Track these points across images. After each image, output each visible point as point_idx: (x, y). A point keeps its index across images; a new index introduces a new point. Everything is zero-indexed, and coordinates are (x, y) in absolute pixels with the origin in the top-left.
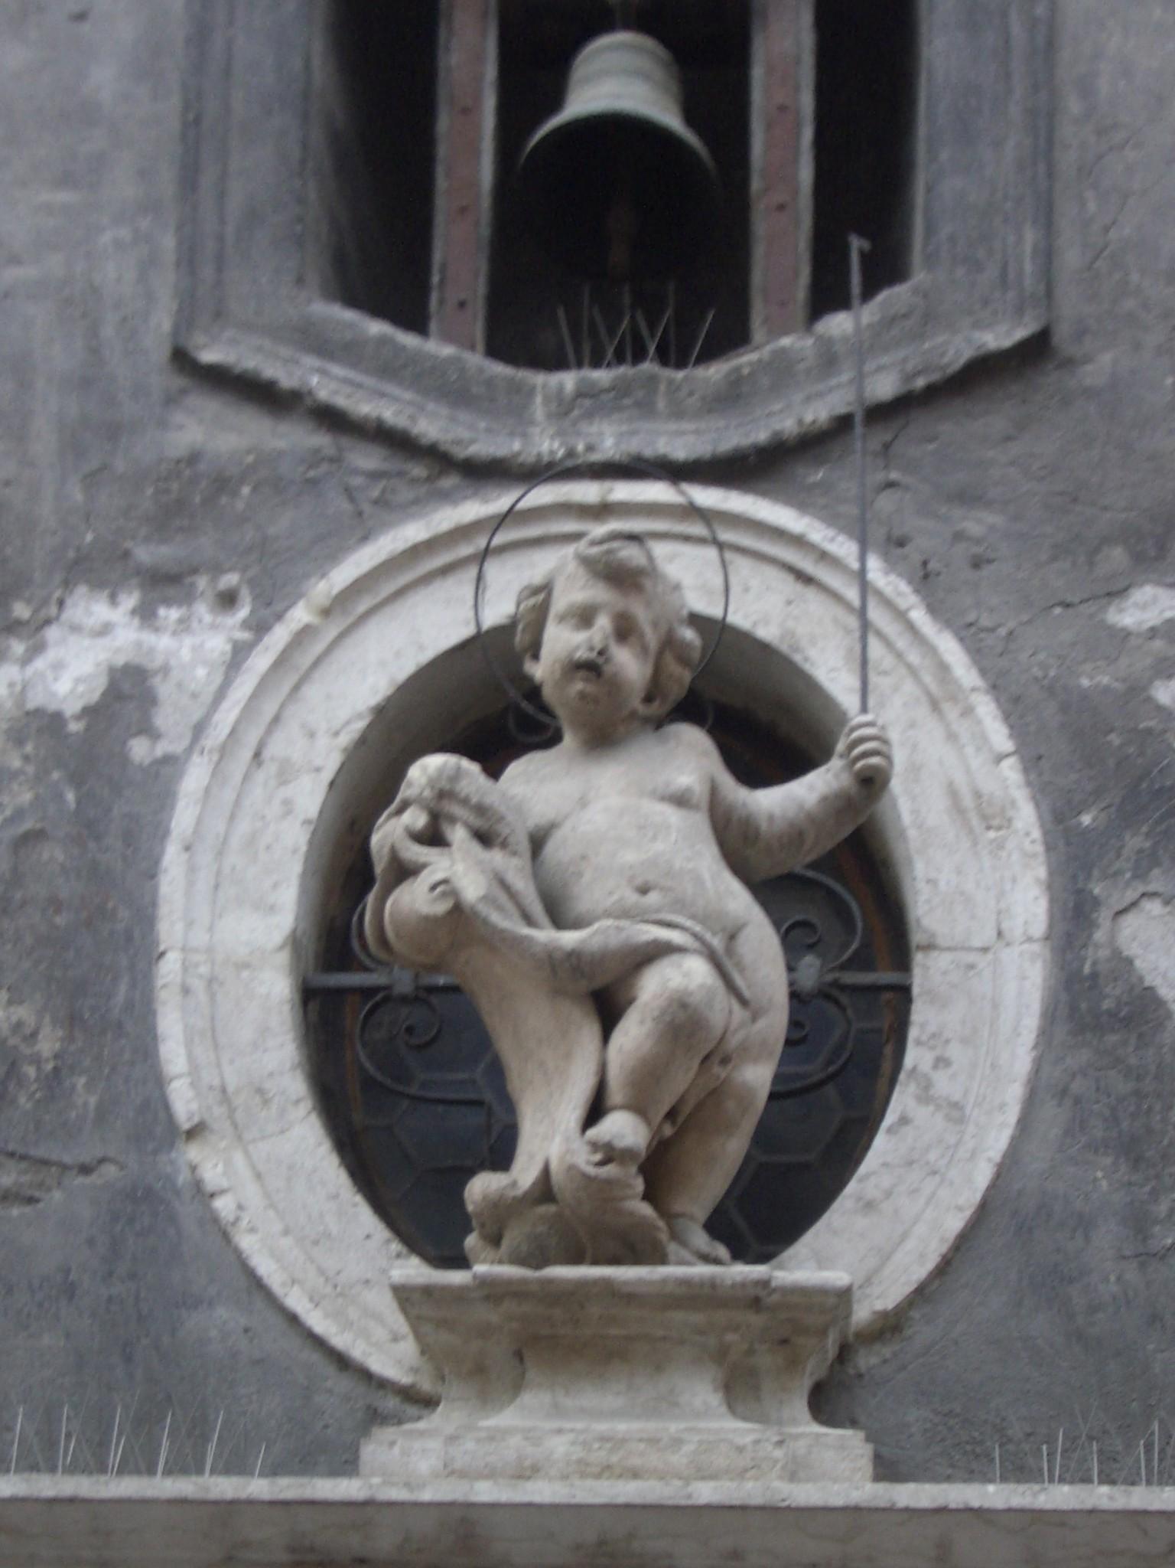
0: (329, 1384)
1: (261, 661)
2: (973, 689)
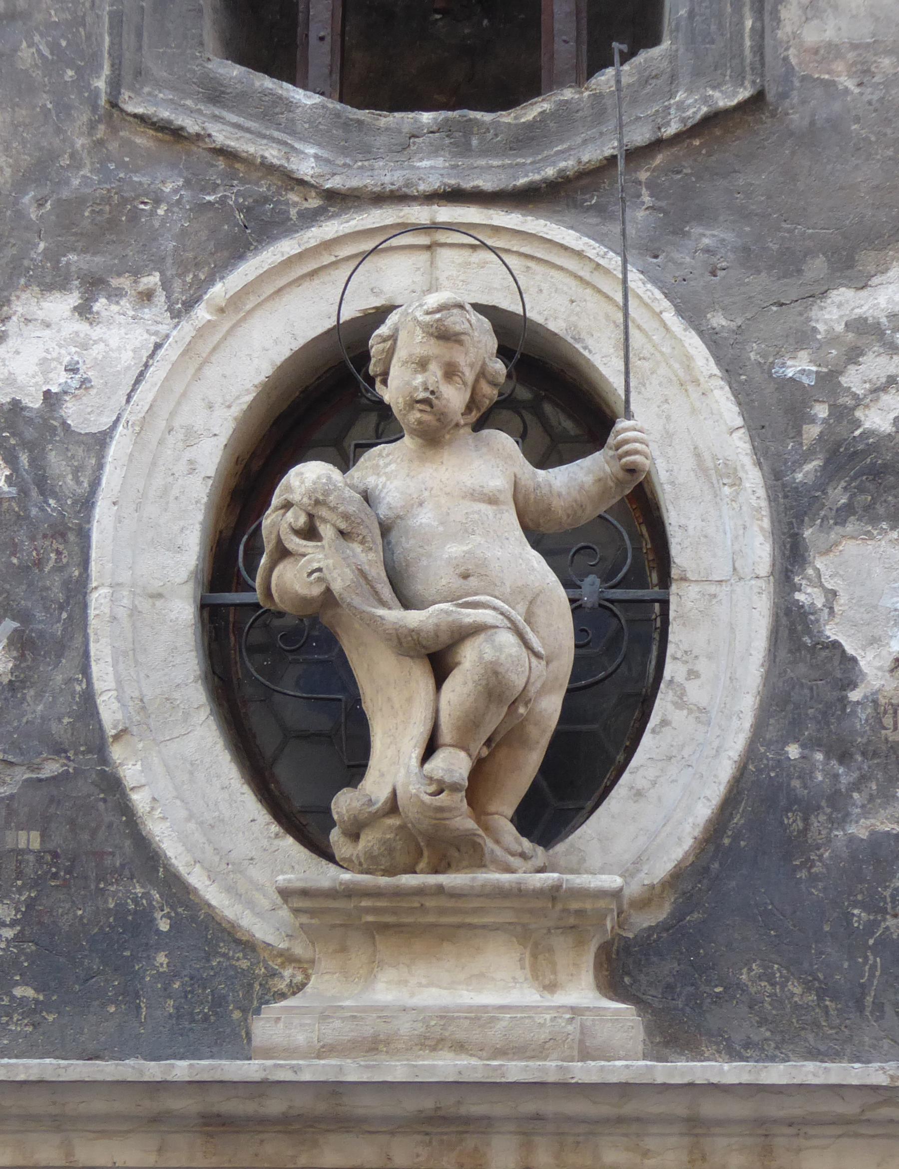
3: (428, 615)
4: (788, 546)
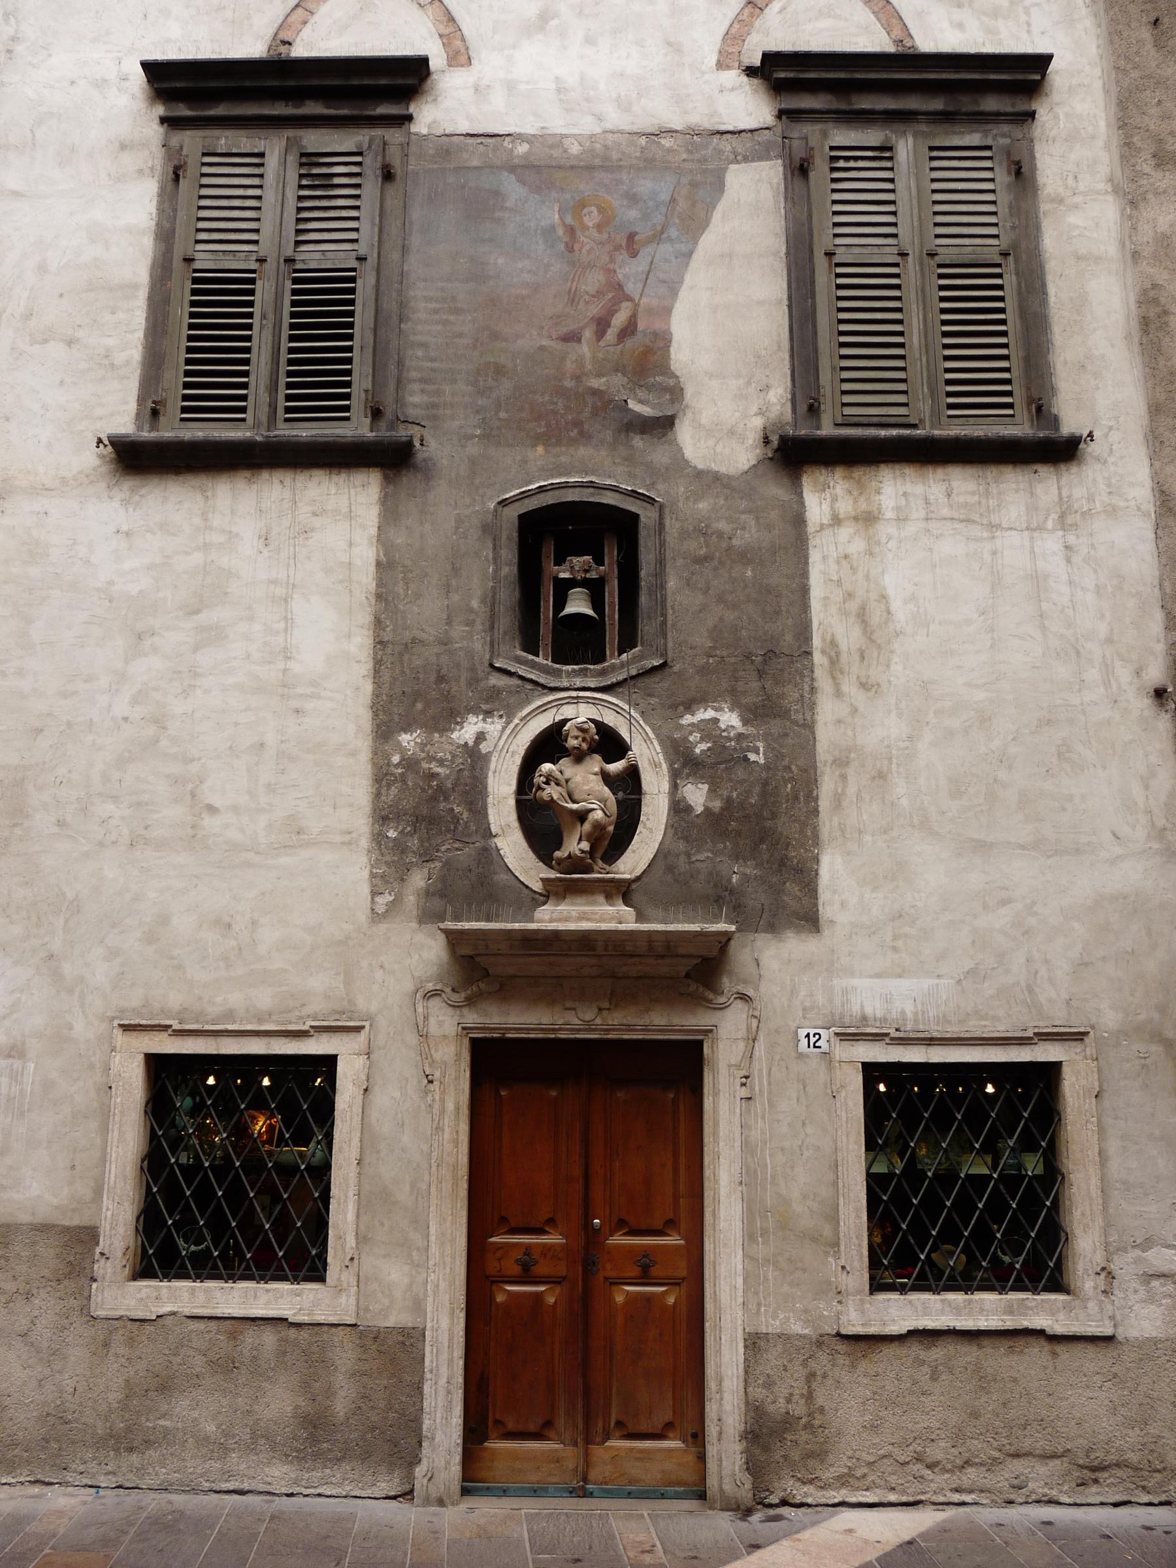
1: (508, 731)
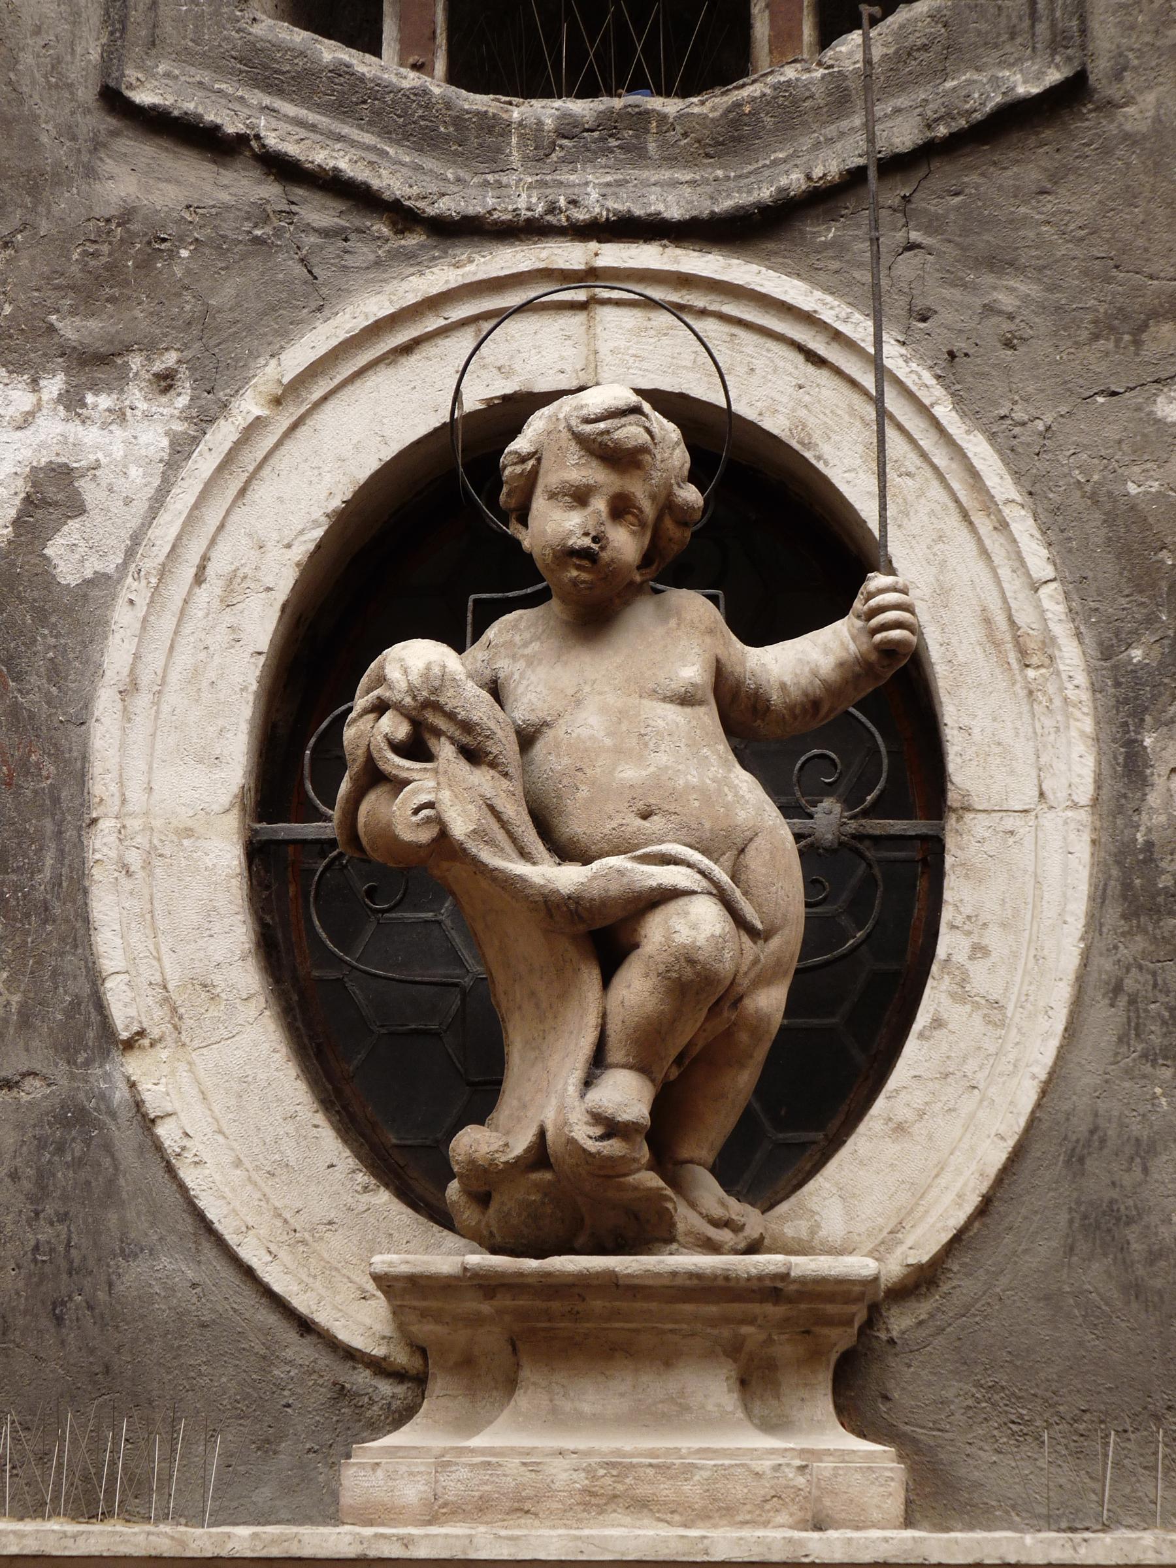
0: (289, 1354)
1: (204, 463)
2: (1008, 501)
3: (590, 874)
4: (1121, 760)
